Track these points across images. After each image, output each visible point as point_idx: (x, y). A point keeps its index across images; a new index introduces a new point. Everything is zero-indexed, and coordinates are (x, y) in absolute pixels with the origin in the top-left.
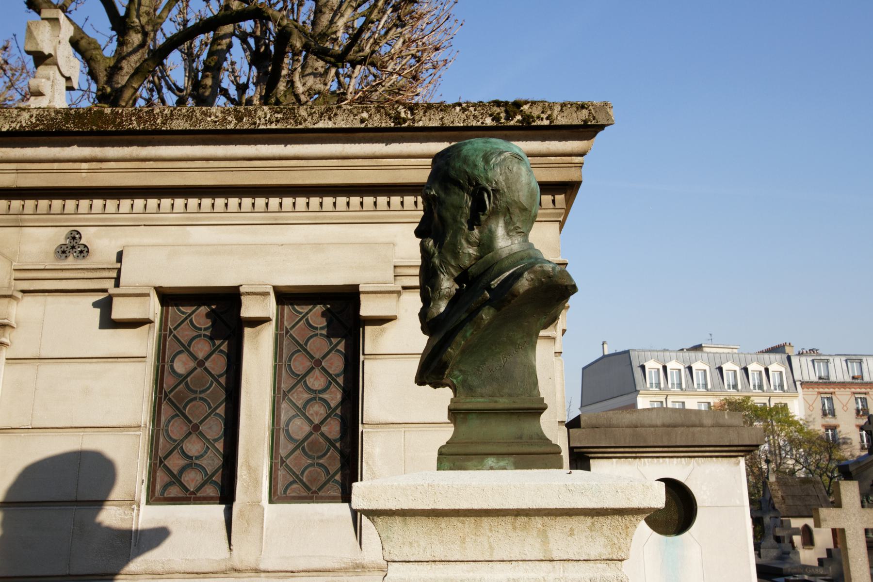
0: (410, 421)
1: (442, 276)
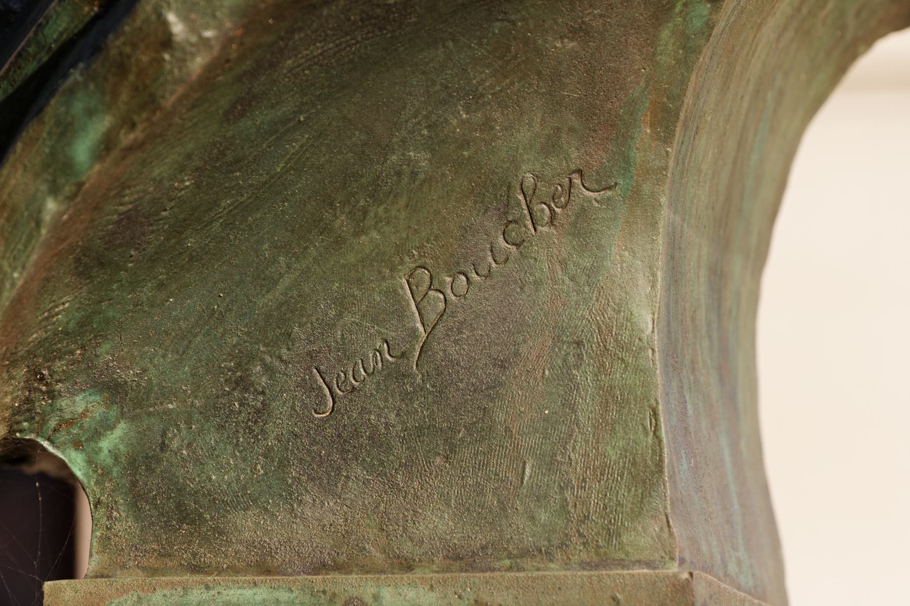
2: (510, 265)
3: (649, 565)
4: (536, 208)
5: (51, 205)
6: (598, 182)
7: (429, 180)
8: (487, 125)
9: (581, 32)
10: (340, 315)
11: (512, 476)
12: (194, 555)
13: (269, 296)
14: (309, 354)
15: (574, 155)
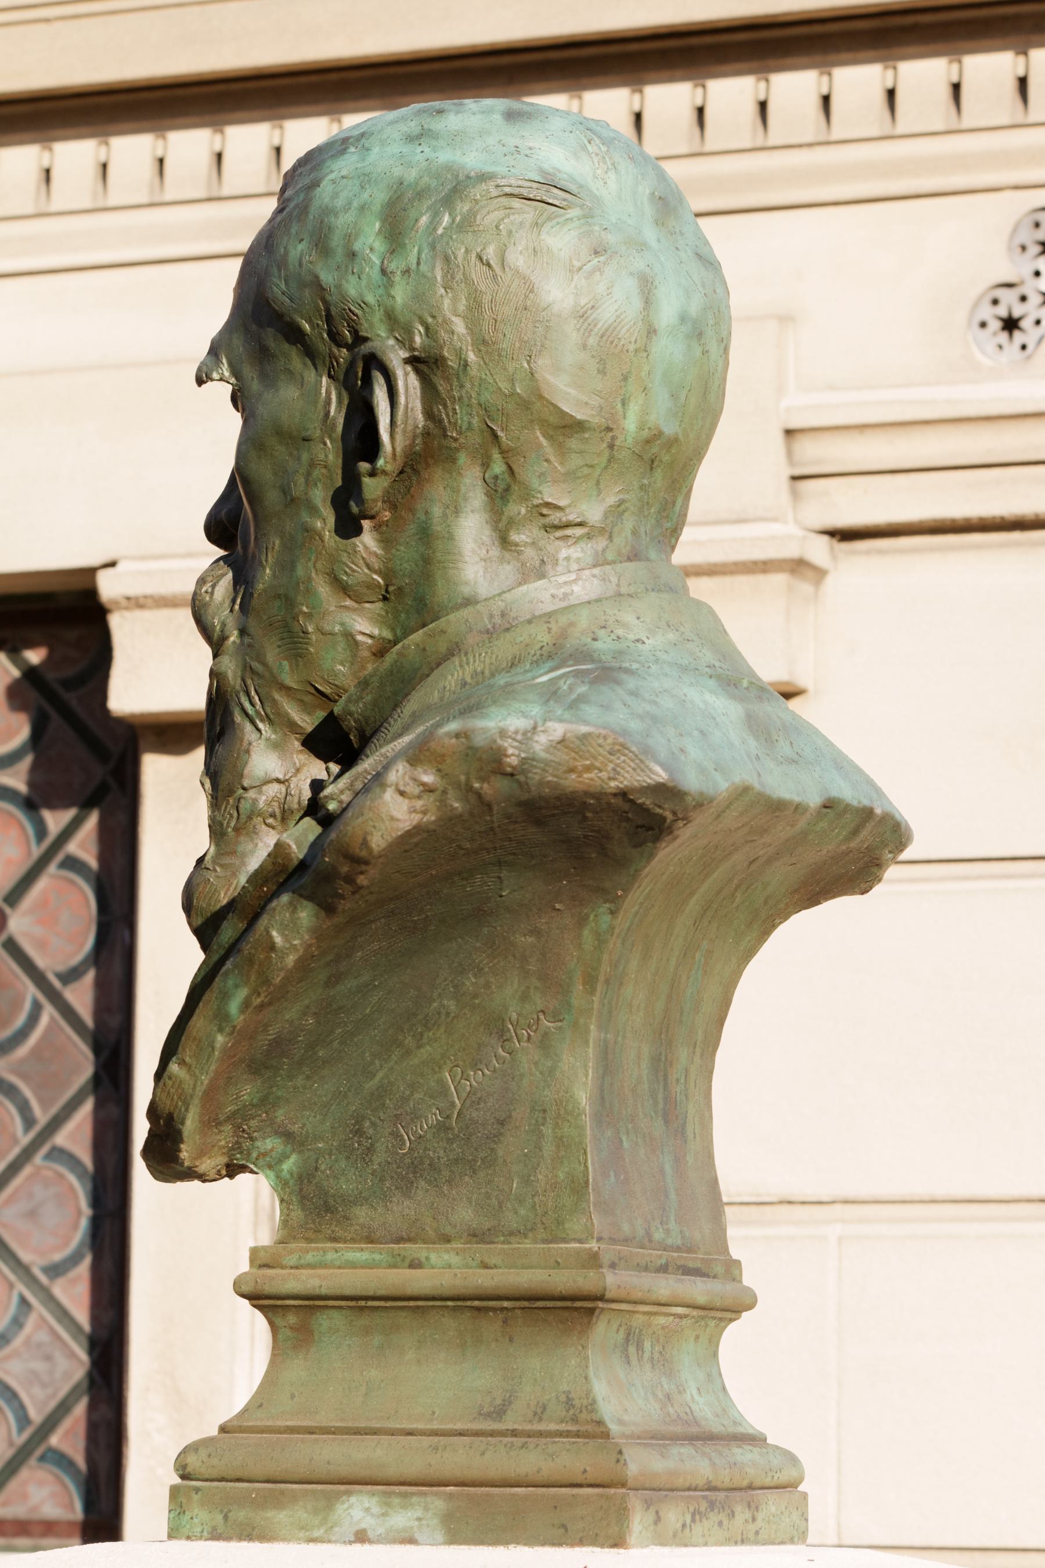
0: (863, 1193)
3: (580, 1241)
5: (220, 1039)
6: (554, 1017)
7: (456, 1017)
8: (487, 985)
9: (536, 932)
10: (412, 1094)
12: (333, 1231)
13: (372, 1083)
14: (396, 1116)
15: (539, 1002)
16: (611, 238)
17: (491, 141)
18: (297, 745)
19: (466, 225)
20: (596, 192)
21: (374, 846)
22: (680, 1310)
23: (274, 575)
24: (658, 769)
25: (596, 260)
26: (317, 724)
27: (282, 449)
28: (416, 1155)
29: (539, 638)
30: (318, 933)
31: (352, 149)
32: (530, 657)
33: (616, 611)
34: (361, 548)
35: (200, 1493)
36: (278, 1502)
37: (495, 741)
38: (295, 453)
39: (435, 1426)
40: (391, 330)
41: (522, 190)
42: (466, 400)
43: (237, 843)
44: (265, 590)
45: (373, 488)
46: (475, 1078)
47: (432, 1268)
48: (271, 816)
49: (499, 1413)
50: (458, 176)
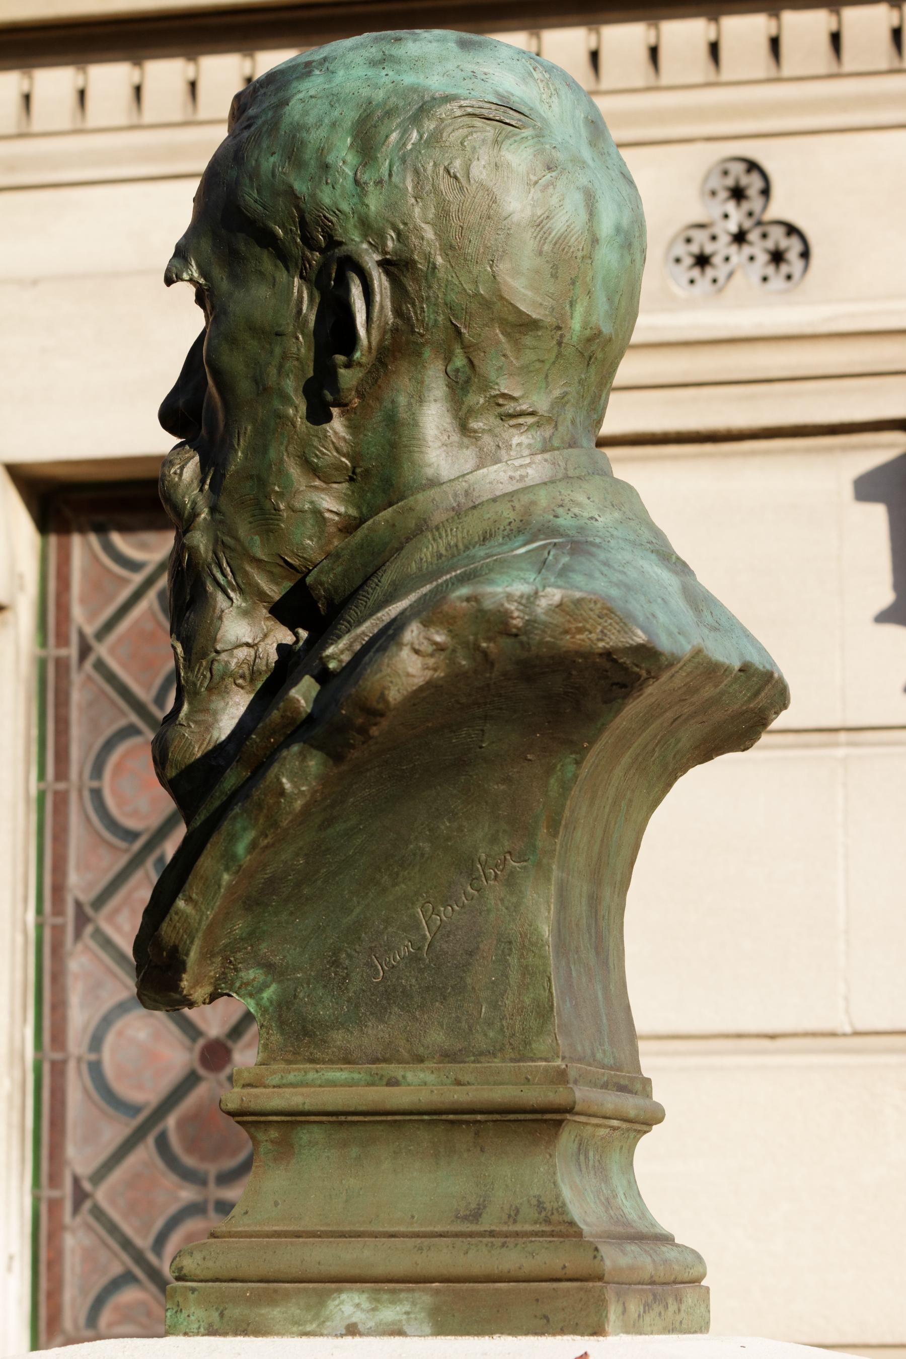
1: (221, 601)
2: (474, 901)
3: (546, 1060)
4: (487, 871)
5: (226, 877)
6: (519, 858)
8: (460, 829)
9: (507, 780)
10: (386, 928)
11: (475, 1013)
12: (311, 1053)
13: (349, 918)
14: (370, 948)
15: (506, 843)
16: (560, 156)
17: (450, 66)
18: (265, 612)
19: (435, 139)
20: (542, 113)
21: (391, 699)
22: (615, 1123)
23: (246, 457)
24: (639, 632)
25: (550, 175)
26: (283, 593)
27: (255, 343)
28: (389, 983)
29: (505, 514)
30: (325, 780)
31: (317, 72)
32: (501, 532)
33: (570, 492)
34: (330, 433)
35: (196, 1293)
36: (272, 1300)
37: (502, 605)
38: (268, 346)
39: (416, 1229)
40: (365, 236)
41: (483, 110)
42: (433, 299)
43: (210, 701)
44: (237, 472)
45: (348, 378)
46: (446, 913)
47: (409, 1085)
48: (241, 677)
49: (475, 1216)
50: (423, 97)
